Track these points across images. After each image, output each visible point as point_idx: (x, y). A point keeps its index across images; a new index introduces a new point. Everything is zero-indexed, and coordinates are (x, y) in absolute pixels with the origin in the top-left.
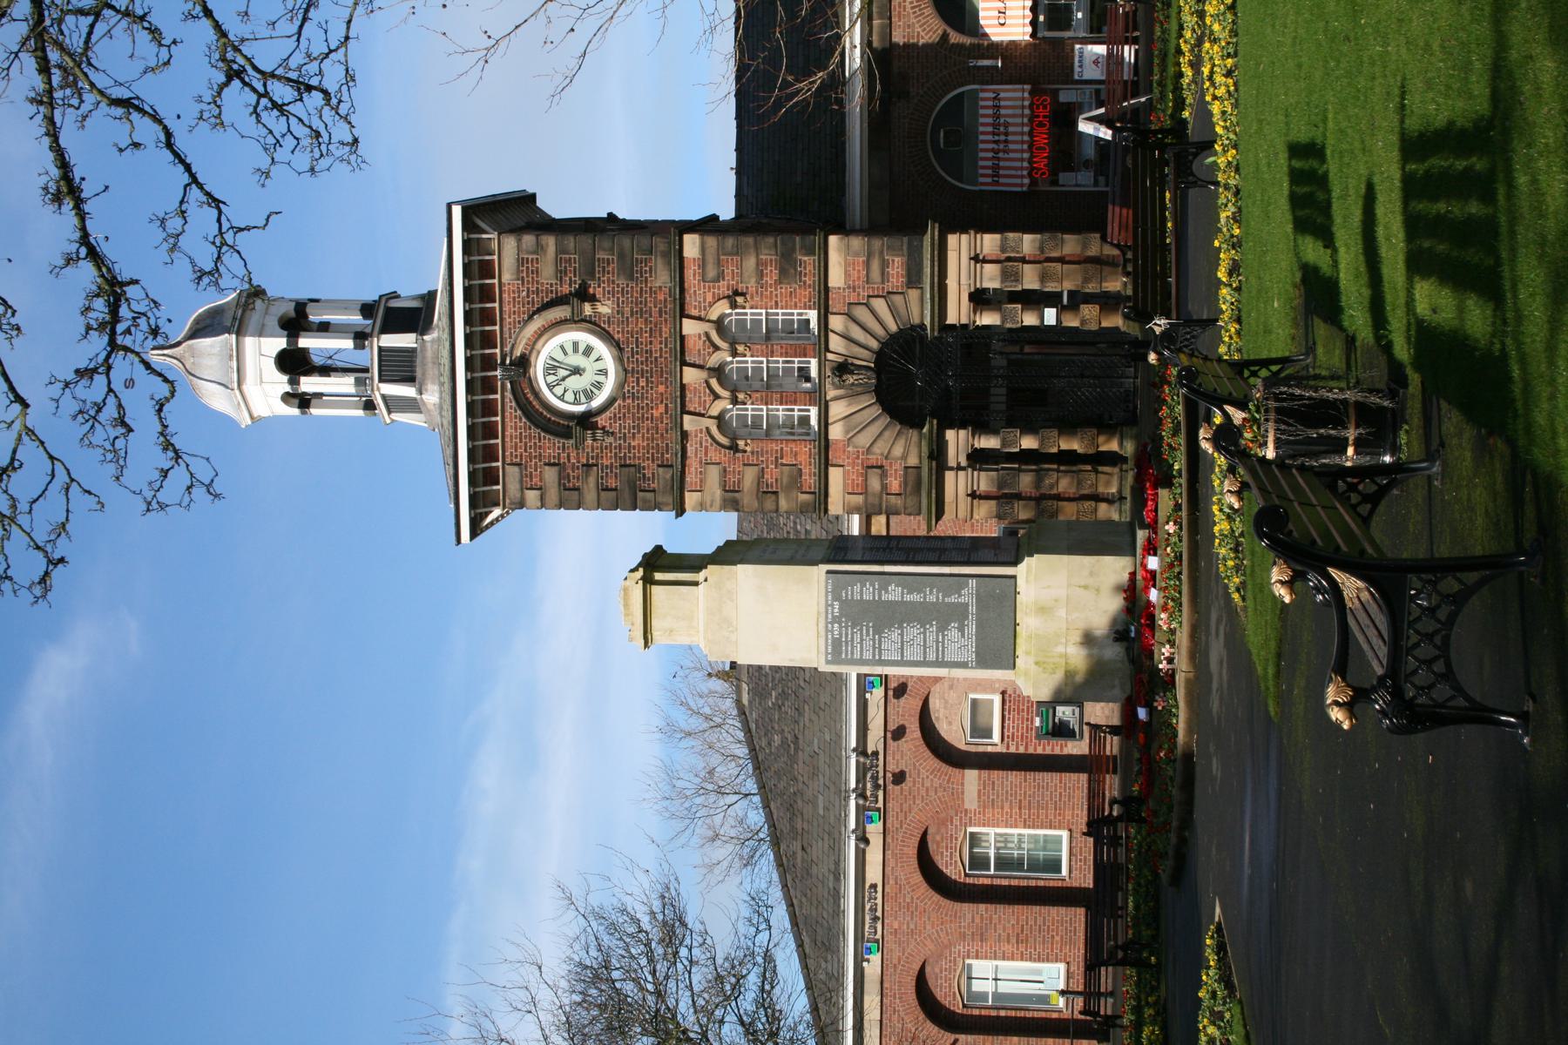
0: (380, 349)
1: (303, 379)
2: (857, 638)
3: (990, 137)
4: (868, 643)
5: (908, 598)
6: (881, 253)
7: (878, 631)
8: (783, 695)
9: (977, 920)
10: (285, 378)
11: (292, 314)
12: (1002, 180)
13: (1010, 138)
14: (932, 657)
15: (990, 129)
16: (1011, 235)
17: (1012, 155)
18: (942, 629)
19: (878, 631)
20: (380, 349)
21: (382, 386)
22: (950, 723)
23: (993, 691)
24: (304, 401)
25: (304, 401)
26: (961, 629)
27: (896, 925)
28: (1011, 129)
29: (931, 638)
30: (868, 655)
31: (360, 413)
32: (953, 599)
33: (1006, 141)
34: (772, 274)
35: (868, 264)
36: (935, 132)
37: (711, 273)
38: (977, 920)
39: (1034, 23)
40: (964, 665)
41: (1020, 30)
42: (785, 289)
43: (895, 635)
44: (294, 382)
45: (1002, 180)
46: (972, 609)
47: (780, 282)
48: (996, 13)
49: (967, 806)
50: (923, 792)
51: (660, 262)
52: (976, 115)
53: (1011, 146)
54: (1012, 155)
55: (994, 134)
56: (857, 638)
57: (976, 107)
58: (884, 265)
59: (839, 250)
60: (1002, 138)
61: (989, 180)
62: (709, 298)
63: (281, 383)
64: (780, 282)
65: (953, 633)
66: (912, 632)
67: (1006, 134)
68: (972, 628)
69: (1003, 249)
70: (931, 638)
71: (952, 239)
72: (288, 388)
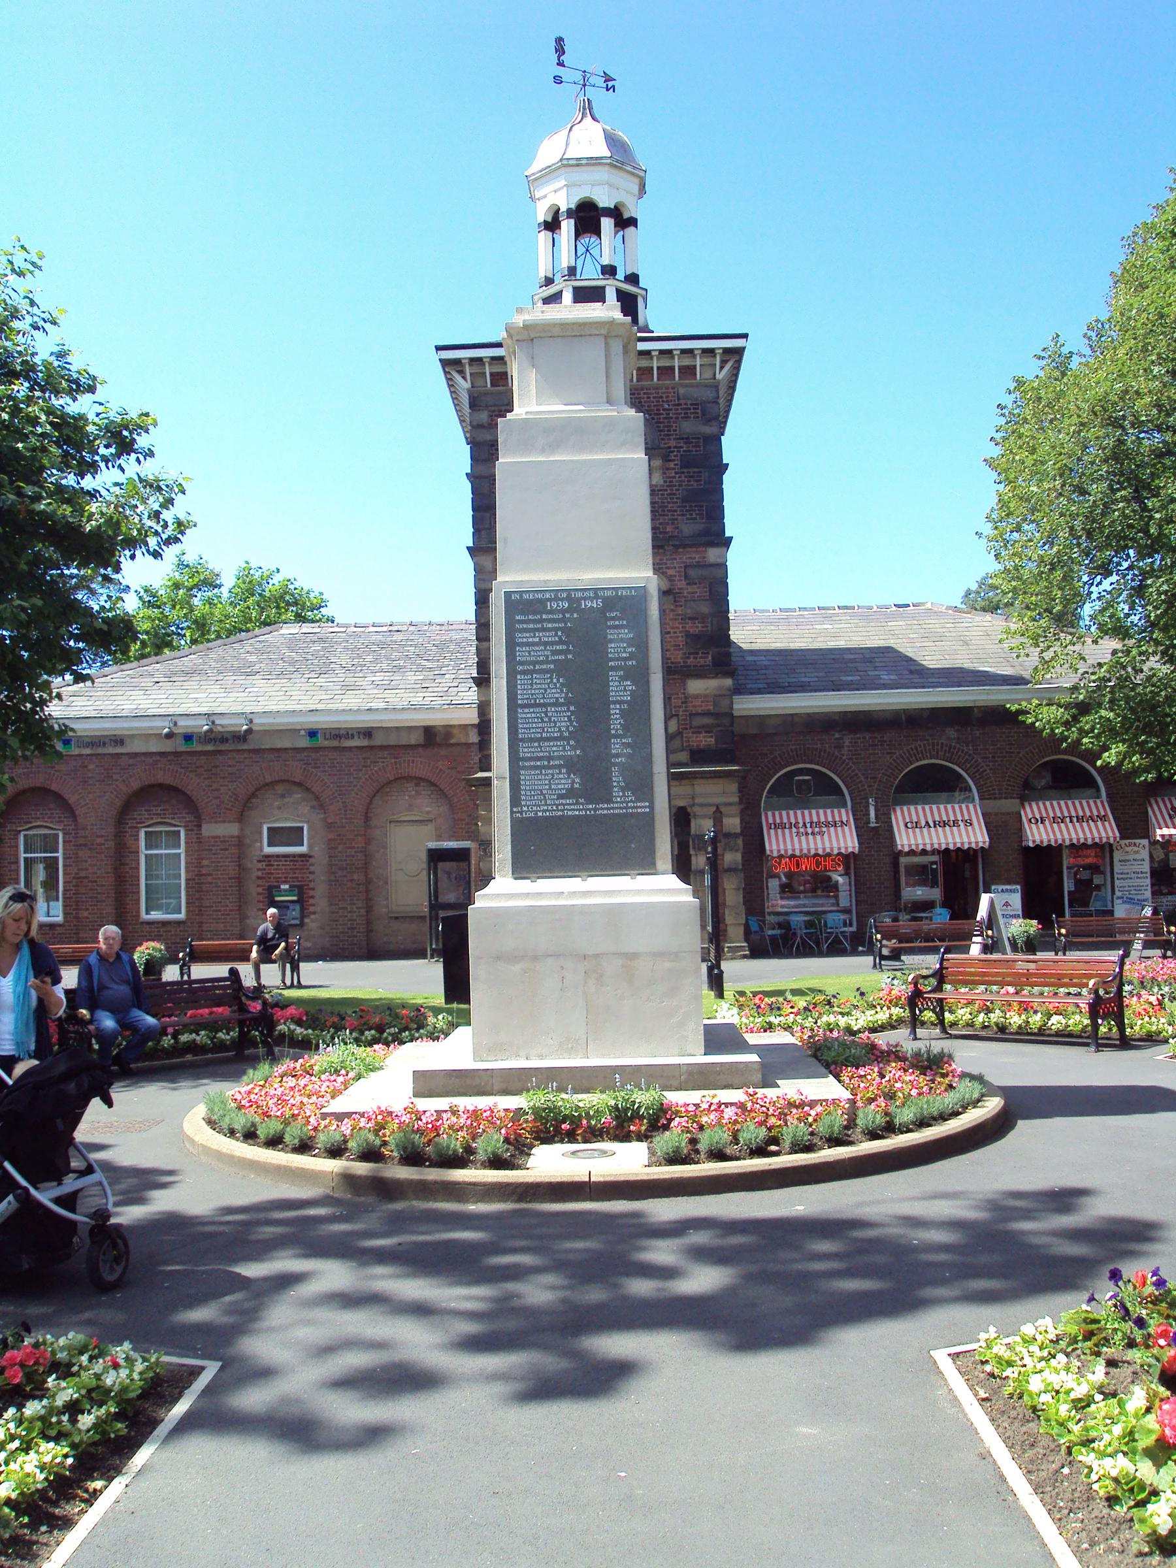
0: (603, 288)
1: (572, 221)
2: (548, 637)
3: (808, 820)
4: (540, 653)
5: (615, 710)
6: (719, 725)
7: (561, 668)
8: (292, 663)
9: (99, 840)
10: (573, 206)
11: (626, 216)
12: (772, 831)
13: (810, 837)
14: (525, 751)
15: (815, 820)
16: (740, 842)
17: (796, 839)
18: (571, 766)
19: (561, 668)
20: (603, 288)
21: (571, 290)
22: (279, 808)
23: (310, 846)
24: (552, 225)
25: (552, 225)
26: (571, 793)
27: (91, 767)
28: (818, 837)
29: (555, 748)
30: (522, 654)
31: (542, 274)
32: (617, 778)
33: (807, 834)
34: (695, 628)
35: (707, 714)
36: (801, 772)
37: (692, 573)
38: (99, 840)
39: (912, 853)
40: (515, 800)
41: (905, 842)
42: (681, 640)
43: (556, 693)
44: (570, 213)
45: (772, 831)
46: (604, 809)
47: (688, 635)
48: (915, 820)
49: (205, 827)
50: (215, 786)
51: (702, 526)
52: (825, 807)
53: (803, 838)
54: (796, 839)
55: (811, 823)
56: (548, 637)
57: (832, 807)
58: (708, 729)
59: (720, 688)
60: (810, 831)
61: (771, 821)
62: (670, 572)
63: (565, 201)
64: (688, 635)
65: (563, 782)
66: (563, 721)
67: (813, 833)
68: (574, 809)
69: (728, 835)
70: (555, 748)
71: (733, 787)
72: (563, 209)
